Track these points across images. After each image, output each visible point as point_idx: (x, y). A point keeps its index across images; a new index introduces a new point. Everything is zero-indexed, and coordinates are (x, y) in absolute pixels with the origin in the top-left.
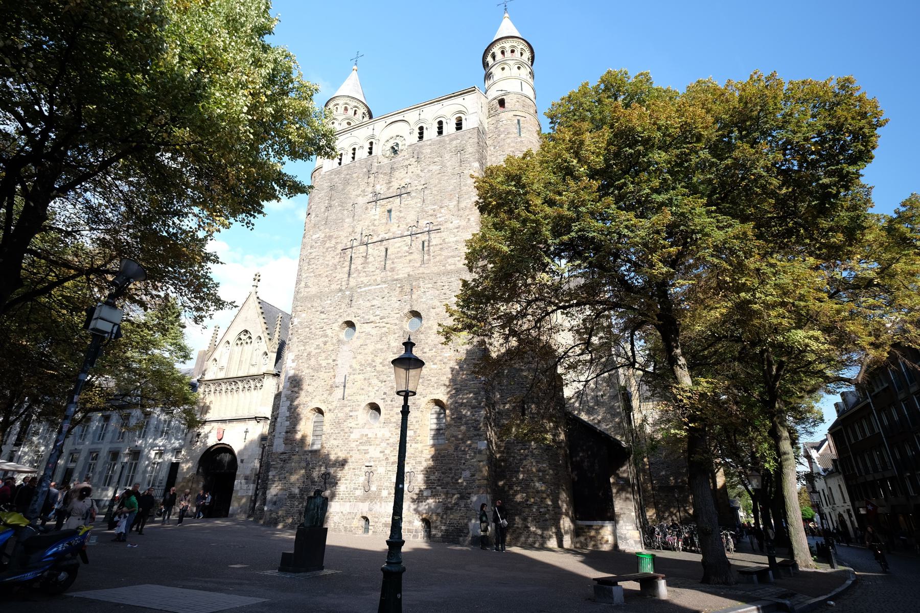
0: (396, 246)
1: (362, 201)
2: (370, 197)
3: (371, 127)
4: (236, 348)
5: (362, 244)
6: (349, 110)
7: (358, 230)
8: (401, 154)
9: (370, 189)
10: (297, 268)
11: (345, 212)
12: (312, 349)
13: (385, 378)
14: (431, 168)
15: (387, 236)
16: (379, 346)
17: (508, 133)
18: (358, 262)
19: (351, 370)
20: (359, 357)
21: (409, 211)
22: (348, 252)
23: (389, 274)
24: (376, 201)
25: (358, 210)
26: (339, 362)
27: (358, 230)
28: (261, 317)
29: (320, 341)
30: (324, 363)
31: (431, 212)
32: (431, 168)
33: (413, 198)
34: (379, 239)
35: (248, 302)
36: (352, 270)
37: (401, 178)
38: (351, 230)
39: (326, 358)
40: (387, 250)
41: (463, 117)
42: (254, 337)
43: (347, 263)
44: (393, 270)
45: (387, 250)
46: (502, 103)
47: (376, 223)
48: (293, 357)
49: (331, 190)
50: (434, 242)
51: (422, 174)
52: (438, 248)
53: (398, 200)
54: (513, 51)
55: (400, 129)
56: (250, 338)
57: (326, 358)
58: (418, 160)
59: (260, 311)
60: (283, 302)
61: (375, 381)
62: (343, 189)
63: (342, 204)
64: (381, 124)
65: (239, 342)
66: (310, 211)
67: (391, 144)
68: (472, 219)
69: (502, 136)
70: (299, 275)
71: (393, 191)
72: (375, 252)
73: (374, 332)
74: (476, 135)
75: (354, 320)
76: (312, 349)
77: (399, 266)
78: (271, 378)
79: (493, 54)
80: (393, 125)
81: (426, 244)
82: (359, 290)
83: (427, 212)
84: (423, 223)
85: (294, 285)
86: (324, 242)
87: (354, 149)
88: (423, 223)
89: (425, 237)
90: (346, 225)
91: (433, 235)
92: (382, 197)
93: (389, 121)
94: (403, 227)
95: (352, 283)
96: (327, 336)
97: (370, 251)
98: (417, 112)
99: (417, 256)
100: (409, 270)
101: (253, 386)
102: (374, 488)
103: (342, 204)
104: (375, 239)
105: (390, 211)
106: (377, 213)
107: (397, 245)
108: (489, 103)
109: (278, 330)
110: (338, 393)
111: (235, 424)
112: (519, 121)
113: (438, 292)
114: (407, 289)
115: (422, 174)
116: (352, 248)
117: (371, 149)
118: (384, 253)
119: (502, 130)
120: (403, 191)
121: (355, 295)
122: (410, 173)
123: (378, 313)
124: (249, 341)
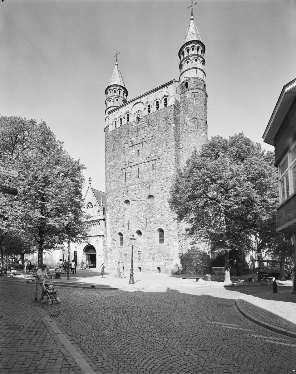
0: (143, 167)
1: (127, 146)
2: (130, 144)
3: (127, 106)
4: (87, 209)
5: (129, 167)
6: (117, 92)
7: (127, 160)
8: (141, 121)
9: (129, 140)
10: (105, 176)
11: (121, 152)
12: (115, 211)
13: (142, 221)
14: (154, 128)
15: (138, 163)
16: (139, 209)
17: (189, 103)
18: (128, 175)
19: (130, 219)
20: (132, 214)
21: (146, 150)
22: (124, 170)
23: (141, 180)
24: (132, 146)
25: (126, 150)
26: (126, 216)
27: (127, 160)
28: (95, 197)
29: (118, 208)
30: (120, 216)
31: (155, 150)
32: (154, 128)
33: (148, 144)
34: (135, 164)
35: (88, 190)
36: (126, 178)
37: (143, 134)
38: (124, 160)
39: (121, 215)
40: (139, 169)
41: (168, 98)
42: (93, 205)
43: (124, 175)
44: (142, 178)
45: (139, 169)
46: (187, 84)
47: (134, 156)
48: (109, 214)
49: (114, 141)
50: (157, 164)
51: (151, 131)
52: (159, 167)
53: (141, 145)
54: (193, 49)
55: (140, 107)
56: (92, 205)
57: (121, 215)
58: (149, 125)
59: (96, 200)
60: (102, 188)
61: (139, 223)
62: (119, 141)
63: (119, 148)
64: (131, 105)
65: (88, 207)
66: (106, 149)
67: (136, 116)
68: (172, 153)
69: (187, 105)
70: (106, 179)
71: (139, 141)
72: (135, 169)
73: (137, 204)
74: (173, 109)
75: (129, 199)
76: (115, 211)
77: (144, 176)
78: (102, 221)
79: (183, 51)
80: (137, 105)
81: (154, 165)
82: (130, 187)
83: (154, 150)
84: (153, 155)
85: (105, 146)
86: (114, 166)
87: (121, 119)
88: (153, 155)
89: (153, 162)
90: (122, 158)
91: (157, 161)
92: (135, 144)
93: (135, 102)
94: (145, 158)
95: (127, 184)
96: (120, 206)
97: (132, 169)
98: (147, 97)
99: (151, 171)
100: (148, 178)
101: (96, 224)
102: (142, 258)
103: (119, 148)
104: (134, 164)
105: (138, 151)
106: (133, 151)
107: (143, 166)
108: (181, 84)
109: (102, 202)
110: (127, 227)
111: (93, 237)
112: (194, 95)
113: (160, 187)
114: (148, 186)
115: (151, 131)
116: (125, 168)
117: (128, 118)
118: (138, 170)
119: (187, 101)
120: (143, 140)
121: (129, 189)
122: (145, 131)
123: (137, 196)
124: (92, 206)
